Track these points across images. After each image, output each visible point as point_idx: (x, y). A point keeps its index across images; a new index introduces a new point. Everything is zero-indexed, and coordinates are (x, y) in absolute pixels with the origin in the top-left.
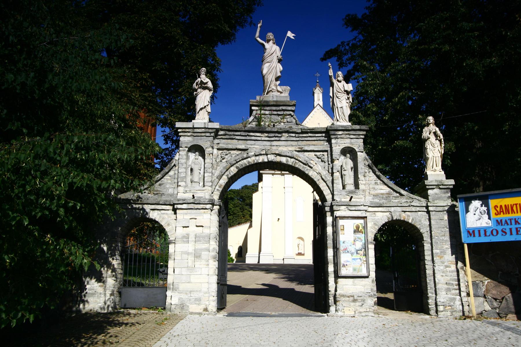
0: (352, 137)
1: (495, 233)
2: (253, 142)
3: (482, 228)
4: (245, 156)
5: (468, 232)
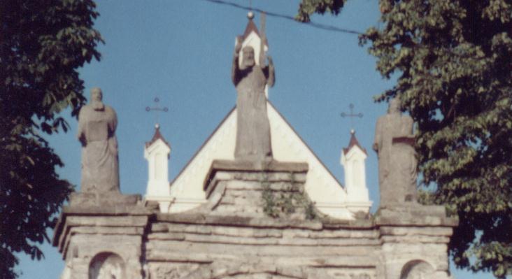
0: (425, 239)
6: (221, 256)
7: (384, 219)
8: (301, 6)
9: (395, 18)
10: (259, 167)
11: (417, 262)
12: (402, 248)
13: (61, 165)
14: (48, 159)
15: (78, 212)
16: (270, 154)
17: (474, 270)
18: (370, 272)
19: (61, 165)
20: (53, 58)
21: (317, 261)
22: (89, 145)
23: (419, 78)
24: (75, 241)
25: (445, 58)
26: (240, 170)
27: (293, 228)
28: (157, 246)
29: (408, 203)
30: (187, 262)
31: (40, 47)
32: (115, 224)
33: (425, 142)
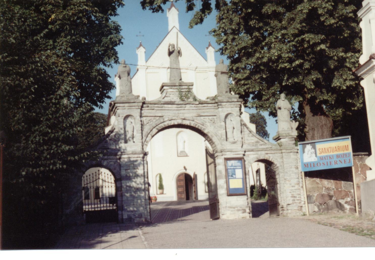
0: (232, 106)
1: (319, 165)
2: (167, 111)
3: (312, 162)
4: (162, 121)
5: (305, 165)
6: (166, 114)
7: (219, 100)
8: (190, 23)
9: (221, 26)
10: (177, 84)
11: (230, 114)
12: (225, 109)
13: (110, 77)
14: (105, 75)
15: (119, 102)
16: (181, 80)
17: (250, 108)
18: (215, 117)
19: (110, 77)
20: (106, 45)
21: (197, 114)
22: (122, 79)
23: (230, 46)
24: (119, 112)
25: (238, 39)
26: (172, 86)
27: (189, 104)
28: (146, 112)
29: (226, 94)
30: (155, 116)
31: (102, 41)
32: (132, 105)
33: (232, 67)
